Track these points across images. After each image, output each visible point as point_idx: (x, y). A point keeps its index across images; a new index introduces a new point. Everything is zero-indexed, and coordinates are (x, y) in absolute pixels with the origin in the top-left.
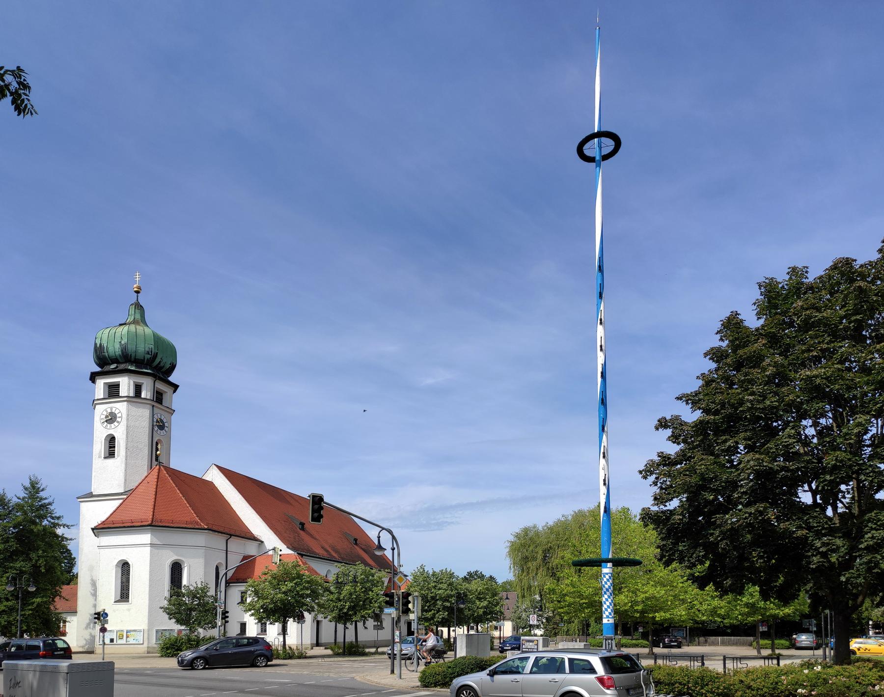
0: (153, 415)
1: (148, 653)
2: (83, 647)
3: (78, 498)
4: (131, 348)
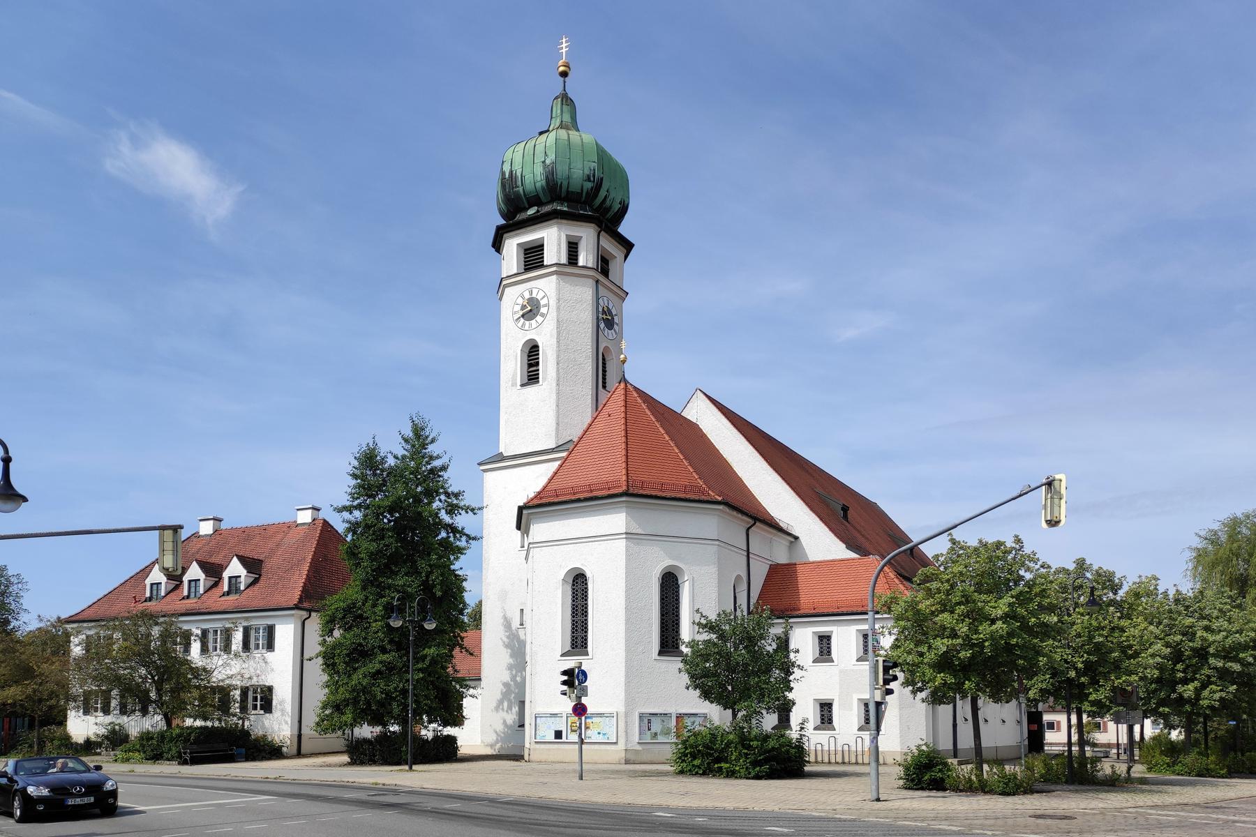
0: (598, 299)
1: (627, 762)
2: (492, 746)
3: (480, 464)
4: (561, 171)
